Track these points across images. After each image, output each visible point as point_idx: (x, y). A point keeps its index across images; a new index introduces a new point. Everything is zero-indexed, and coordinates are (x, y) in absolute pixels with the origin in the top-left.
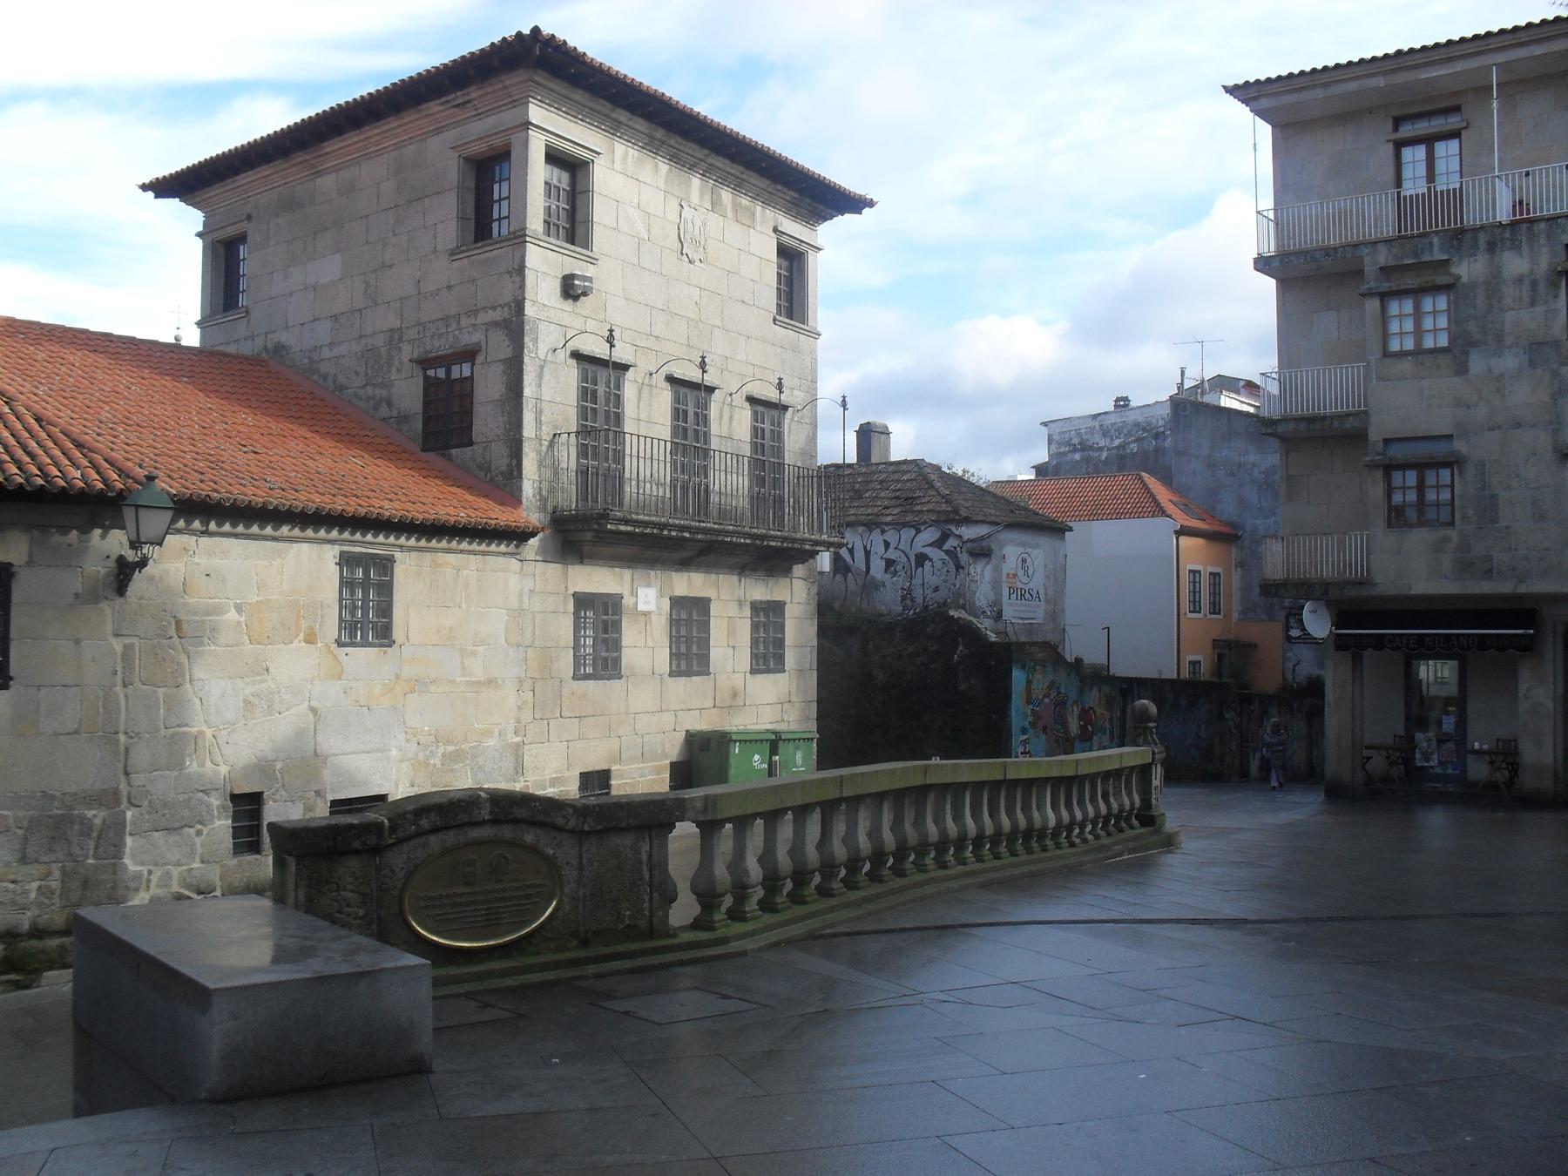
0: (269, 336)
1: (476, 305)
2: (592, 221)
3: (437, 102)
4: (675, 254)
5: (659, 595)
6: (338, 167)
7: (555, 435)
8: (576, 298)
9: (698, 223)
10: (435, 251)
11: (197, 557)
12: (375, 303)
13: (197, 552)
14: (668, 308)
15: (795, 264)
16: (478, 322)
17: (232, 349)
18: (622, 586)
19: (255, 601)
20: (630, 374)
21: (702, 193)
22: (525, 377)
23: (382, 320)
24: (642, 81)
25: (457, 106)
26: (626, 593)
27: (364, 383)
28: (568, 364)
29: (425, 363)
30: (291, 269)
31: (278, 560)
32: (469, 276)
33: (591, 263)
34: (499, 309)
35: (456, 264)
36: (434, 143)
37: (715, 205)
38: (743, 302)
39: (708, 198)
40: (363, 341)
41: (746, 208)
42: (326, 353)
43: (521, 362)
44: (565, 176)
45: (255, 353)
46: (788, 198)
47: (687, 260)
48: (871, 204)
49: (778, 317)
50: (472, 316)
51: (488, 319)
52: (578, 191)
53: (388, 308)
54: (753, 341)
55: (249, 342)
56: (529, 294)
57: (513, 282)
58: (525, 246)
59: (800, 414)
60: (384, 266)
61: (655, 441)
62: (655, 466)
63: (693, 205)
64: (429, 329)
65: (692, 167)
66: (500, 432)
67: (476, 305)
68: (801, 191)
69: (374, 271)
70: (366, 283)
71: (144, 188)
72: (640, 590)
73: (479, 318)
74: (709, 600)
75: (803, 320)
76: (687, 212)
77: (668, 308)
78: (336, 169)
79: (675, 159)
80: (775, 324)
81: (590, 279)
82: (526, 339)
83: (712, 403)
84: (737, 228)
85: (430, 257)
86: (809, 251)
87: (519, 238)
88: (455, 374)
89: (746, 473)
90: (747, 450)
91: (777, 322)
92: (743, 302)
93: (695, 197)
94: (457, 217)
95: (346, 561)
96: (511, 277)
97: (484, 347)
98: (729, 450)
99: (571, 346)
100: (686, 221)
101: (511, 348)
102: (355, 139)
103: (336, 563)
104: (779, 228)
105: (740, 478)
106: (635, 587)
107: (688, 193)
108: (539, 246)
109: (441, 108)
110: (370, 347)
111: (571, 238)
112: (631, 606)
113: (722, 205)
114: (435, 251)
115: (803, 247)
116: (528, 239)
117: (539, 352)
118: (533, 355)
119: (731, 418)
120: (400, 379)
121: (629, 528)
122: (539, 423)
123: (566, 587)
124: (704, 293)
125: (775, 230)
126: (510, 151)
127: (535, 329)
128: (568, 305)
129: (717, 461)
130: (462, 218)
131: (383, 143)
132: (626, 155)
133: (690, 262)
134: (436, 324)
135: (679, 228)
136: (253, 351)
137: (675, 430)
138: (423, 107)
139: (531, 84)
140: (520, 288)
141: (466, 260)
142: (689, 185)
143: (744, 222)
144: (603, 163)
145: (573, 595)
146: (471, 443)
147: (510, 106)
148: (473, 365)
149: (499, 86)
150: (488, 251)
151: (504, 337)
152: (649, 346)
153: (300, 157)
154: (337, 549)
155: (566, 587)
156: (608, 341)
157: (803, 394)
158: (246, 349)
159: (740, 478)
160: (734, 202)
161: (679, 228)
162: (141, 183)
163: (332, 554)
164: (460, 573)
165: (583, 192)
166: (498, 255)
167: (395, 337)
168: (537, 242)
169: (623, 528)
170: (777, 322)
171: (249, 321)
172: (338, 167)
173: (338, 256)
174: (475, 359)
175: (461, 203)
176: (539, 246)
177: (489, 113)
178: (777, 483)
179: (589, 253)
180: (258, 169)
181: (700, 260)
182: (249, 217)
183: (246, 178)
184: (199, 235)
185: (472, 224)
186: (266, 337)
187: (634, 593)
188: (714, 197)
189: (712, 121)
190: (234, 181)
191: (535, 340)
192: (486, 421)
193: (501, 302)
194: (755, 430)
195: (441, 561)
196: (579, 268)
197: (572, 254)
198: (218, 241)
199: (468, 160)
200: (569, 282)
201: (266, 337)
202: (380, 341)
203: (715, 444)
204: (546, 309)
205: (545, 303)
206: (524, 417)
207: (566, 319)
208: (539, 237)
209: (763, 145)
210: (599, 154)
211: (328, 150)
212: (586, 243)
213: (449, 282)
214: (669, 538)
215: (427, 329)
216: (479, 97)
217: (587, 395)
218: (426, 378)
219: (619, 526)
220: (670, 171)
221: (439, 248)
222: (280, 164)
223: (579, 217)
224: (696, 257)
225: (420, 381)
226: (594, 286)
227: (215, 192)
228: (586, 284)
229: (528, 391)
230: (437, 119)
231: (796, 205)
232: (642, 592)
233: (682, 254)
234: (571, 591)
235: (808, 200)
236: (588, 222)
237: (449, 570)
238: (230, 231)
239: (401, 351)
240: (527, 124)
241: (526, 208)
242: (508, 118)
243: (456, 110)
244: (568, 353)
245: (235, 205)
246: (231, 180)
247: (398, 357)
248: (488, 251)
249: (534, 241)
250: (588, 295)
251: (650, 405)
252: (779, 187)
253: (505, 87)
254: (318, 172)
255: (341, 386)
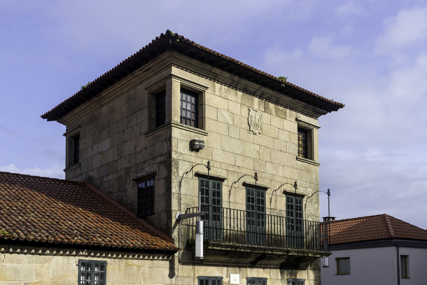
0: (87, 174)
1: (155, 155)
2: (205, 117)
3: (138, 70)
4: (246, 131)
5: (241, 277)
6: (108, 102)
7: (187, 209)
8: (197, 150)
9: (258, 117)
10: (141, 134)
11: (4, 263)
12: (122, 158)
13: (4, 260)
14: (243, 154)
15: (308, 134)
16: (156, 162)
17: (75, 180)
18: (222, 273)
19: (35, 282)
20: (225, 183)
21: (259, 105)
22: (172, 184)
23: (124, 164)
24: (276, 77)
25: (146, 71)
26: (224, 276)
27: (118, 191)
28: (194, 178)
29: (138, 180)
30: (94, 146)
31: (47, 264)
32: (152, 143)
33: (205, 135)
34: (163, 156)
35: (148, 138)
36: (140, 88)
37: (266, 110)
38: (281, 151)
39: (262, 106)
40: (117, 173)
41: (282, 110)
42: (105, 179)
43: (171, 178)
44: (193, 99)
45: (83, 181)
46: (302, 105)
47: (252, 133)
48: (341, 106)
49: (298, 157)
50: (154, 160)
51: (159, 161)
52: (199, 104)
53: (125, 159)
54: (286, 168)
55: (81, 176)
56: (174, 148)
57: (168, 144)
58: (171, 129)
59: (311, 198)
60: (124, 142)
61: (239, 212)
62: (239, 222)
63: (255, 110)
64: (139, 167)
65: (253, 94)
66: (164, 208)
67: (155, 155)
68: (308, 102)
69: (121, 144)
70: (118, 149)
71: (43, 117)
72: (231, 275)
73: (156, 160)
74: (266, 279)
75: (312, 158)
76: (252, 113)
77: (243, 154)
78: (108, 103)
79: (245, 91)
80: (297, 160)
81: (203, 142)
82: (173, 168)
83: (266, 194)
84: (277, 119)
85: (139, 136)
86: (314, 128)
87: (169, 126)
88: (148, 185)
89: (284, 224)
90: (284, 214)
91: (298, 159)
92: (281, 151)
93: (256, 106)
94: (148, 119)
95: (82, 264)
96: (167, 142)
97: (158, 173)
98: (275, 215)
99: (195, 170)
100: (252, 117)
101: (167, 172)
102: (112, 90)
103: (76, 265)
104: (298, 119)
105: (282, 226)
106: (229, 274)
107: (253, 104)
108: (178, 128)
109: (140, 72)
110: (120, 176)
111: (196, 126)
112: (227, 282)
113: (269, 109)
114: (141, 134)
115: (311, 127)
116: (172, 125)
117: (179, 173)
118: (176, 175)
119: (276, 200)
120: (130, 188)
121: (219, 248)
122: (180, 204)
123: (194, 274)
124: (261, 147)
125: (296, 120)
126: (166, 89)
127: (177, 164)
128: (193, 153)
129: (268, 220)
130: (150, 119)
131: (122, 90)
132: (221, 89)
133: (254, 134)
134: (141, 164)
135: (248, 120)
136: (82, 180)
137: (248, 206)
138: (134, 73)
139: (172, 57)
140: (170, 146)
141: (151, 137)
142: (253, 101)
143: (281, 116)
144: (209, 92)
145: (198, 278)
146: (154, 214)
147: (166, 68)
148: (154, 180)
149: (160, 60)
150: (159, 132)
151: (164, 168)
152: (234, 170)
153: (95, 99)
154: (77, 258)
155: (194, 274)
156: (207, 167)
157: (312, 190)
158: (80, 179)
159: (282, 226)
160: (275, 108)
161: (248, 120)
162: (41, 115)
163: (74, 261)
164: (140, 268)
165: (201, 105)
166: (161, 132)
167: (128, 170)
168: (177, 126)
169: (215, 248)
170: (298, 159)
171: (81, 168)
172: (108, 102)
173: (109, 139)
174: (155, 178)
175: (150, 112)
176: (178, 128)
177: (158, 73)
178: (299, 229)
179: (204, 131)
180: (81, 106)
181: (259, 133)
182: (80, 126)
183: (77, 110)
184: (65, 135)
185: (154, 121)
186: (86, 174)
187: (228, 276)
188: (266, 106)
189: (328, 100)
190: (74, 112)
191: (177, 168)
192: (159, 205)
193: (163, 153)
194: (288, 206)
195: (130, 264)
196: (197, 137)
197: (195, 131)
198: (72, 137)
199: (152, 94)
200: (193, 143)
201: (86, 174)
202: (123, 173)
203: (268, 212)
204: (182, 155)
205: (182, 152)
206: (172, 201)
207: (193, 159)
208: (178, 124)
209: (325, 98)
210: (207, 88)
211: (104, 95)
212: (202, 126)
213: (146, 146)
214: (239, 252)
215: (138, 167)
216: (154, 66)
217: (203, 191)
218: (139, 188)
219: (214, 247)
220: (244, 95)
221: (142, 132)
222: (88, 103)
223: (200, 116)
224: (257, 132)
225: (136, 188)
226: (205, 145)
227: (67, 117)
228: (201, 144)
229: (174, 189)
230: (140, 77)
231: (306, 108)
232: (232, 276)
233: (250, 131)
234: (197, 275)
235: (311, 106)
236: (203, 118)
237: (135, 267)
238: (75, 132)
239: (130, 177)
240: (171, 76)
241: (172, 112)
242: (164, 73)
243: (146, 73)
244: (194, 174)
245: (76, 122)
246: (73, 111)
247: (129, 179)
248: (159, 132)
249: (175, 126)
250: (202, 149)
251: (235, 195)
252: (297, 101)
253: (162, 60)
254: (102, 105)
255: (110, 192)
